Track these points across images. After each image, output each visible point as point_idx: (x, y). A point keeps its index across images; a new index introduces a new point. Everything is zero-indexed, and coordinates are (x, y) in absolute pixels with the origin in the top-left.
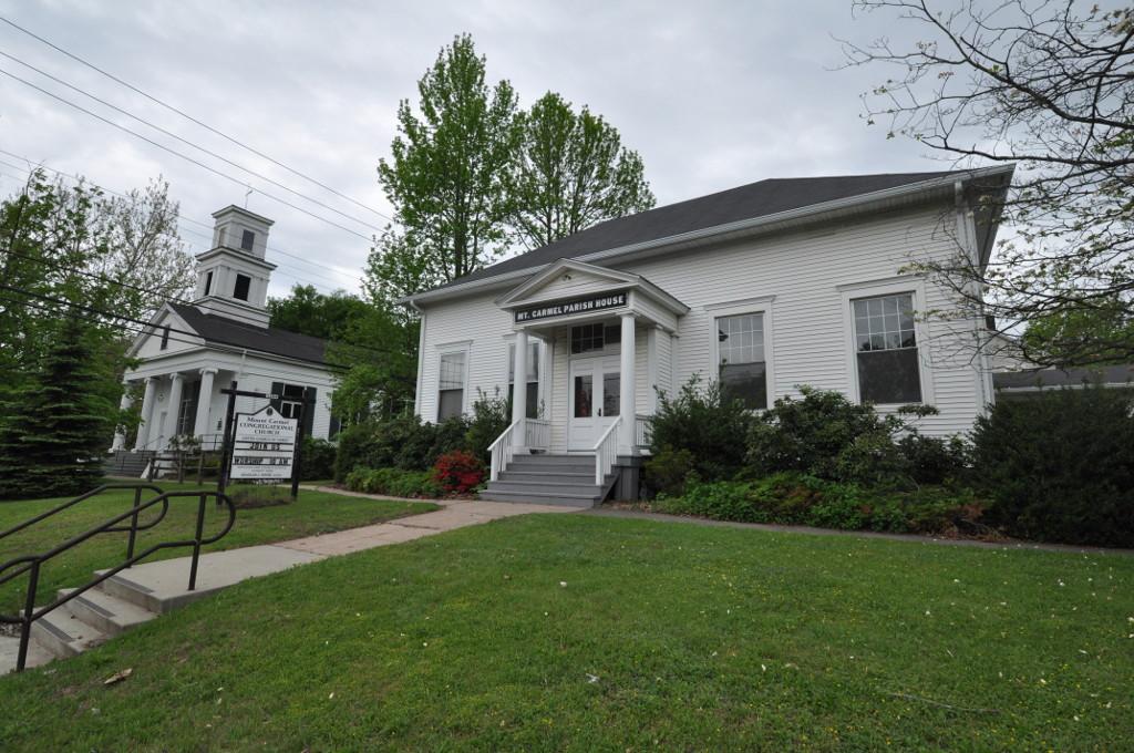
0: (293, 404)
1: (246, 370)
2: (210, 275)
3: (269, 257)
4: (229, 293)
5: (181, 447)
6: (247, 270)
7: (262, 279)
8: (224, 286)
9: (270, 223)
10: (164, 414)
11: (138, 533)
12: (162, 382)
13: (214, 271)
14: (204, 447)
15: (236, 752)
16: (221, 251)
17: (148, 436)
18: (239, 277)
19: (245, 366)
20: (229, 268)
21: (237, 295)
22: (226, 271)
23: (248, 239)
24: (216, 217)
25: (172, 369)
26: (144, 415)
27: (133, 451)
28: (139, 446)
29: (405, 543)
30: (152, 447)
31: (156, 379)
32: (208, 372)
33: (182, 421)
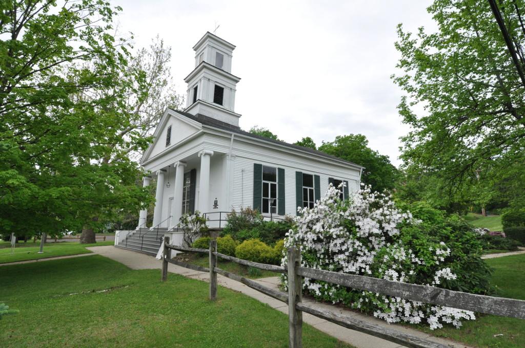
0: (262, 198)
1: (235, 153)
2: (196, 89)
3: (234, 72)
4: (210, 99)
5: (190, 226)
6: (222, 82)
7: (231, 89)
8: (204, 93)
9: (232, 48)
10: (172, 199)
11: (219, 219)
12: (168, 173)
13: (199, 84)
14: (211, 225)
15: (0, 70)
16: (203, 66)
17: (161, 217)
18: (216, 86)
19: (233, 149)
20: (209, 79)
21: (215, 101)
22: (206, 81)
23: (220, 58)
24: (187, 82)
25: (175, 159)
26: (157, 197)
27: (151, 229)
28: (155, 225)
29: (321, 331)
30: (164, 225)
31: (164, 170)
32: (206, 154)
33: (184, 203)
